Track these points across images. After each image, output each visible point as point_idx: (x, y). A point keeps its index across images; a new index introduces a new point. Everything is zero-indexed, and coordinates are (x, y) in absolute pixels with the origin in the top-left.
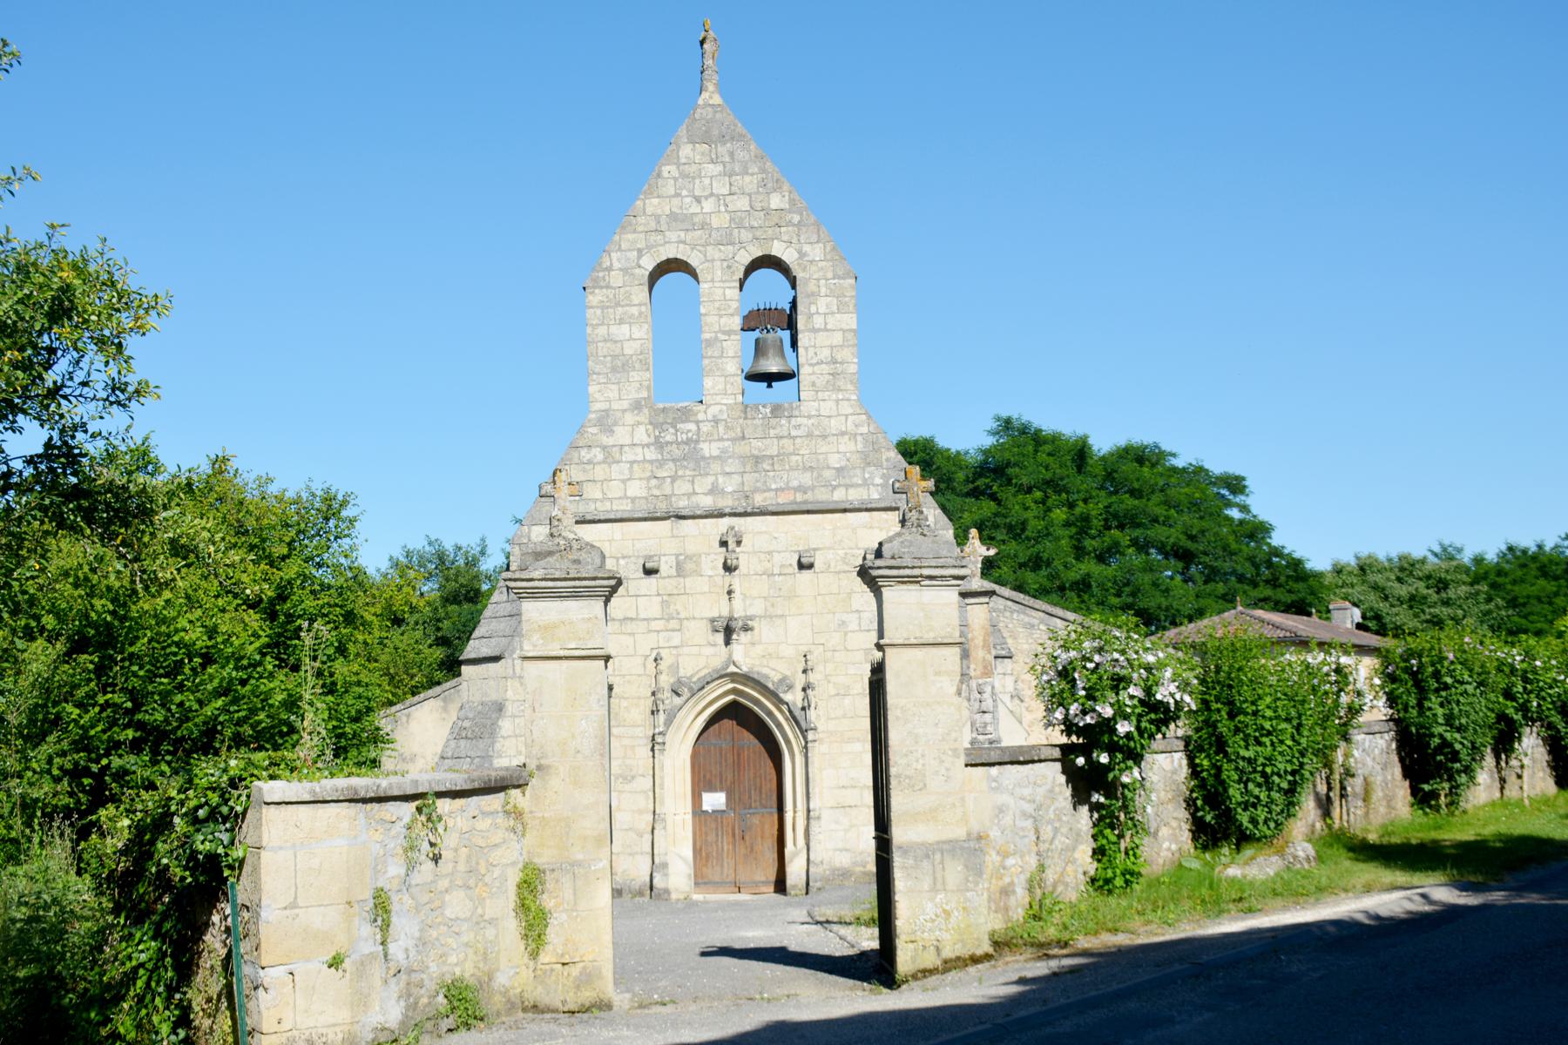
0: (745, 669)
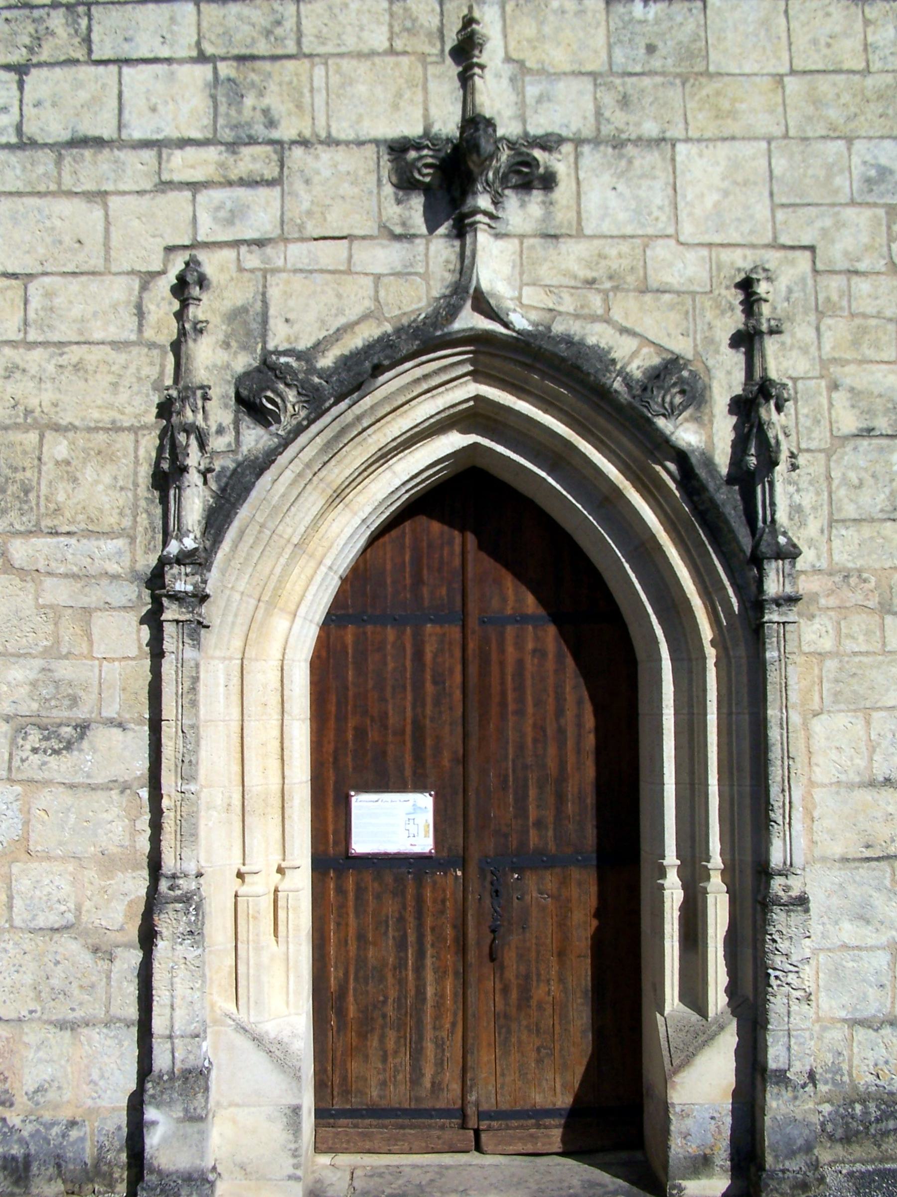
0: (520, 322)
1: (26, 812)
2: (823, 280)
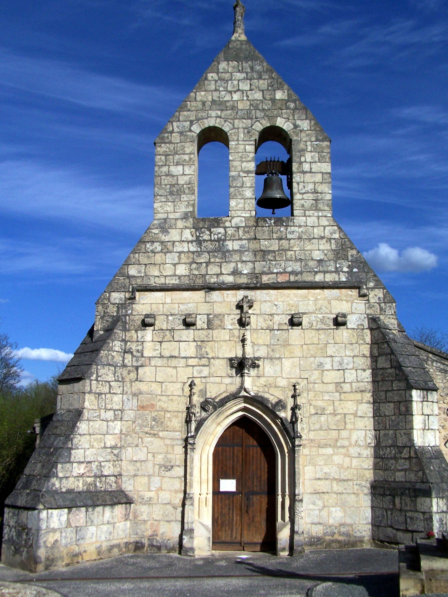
0: (252, 394)
1: (161, 482)
2: (309, 384)
